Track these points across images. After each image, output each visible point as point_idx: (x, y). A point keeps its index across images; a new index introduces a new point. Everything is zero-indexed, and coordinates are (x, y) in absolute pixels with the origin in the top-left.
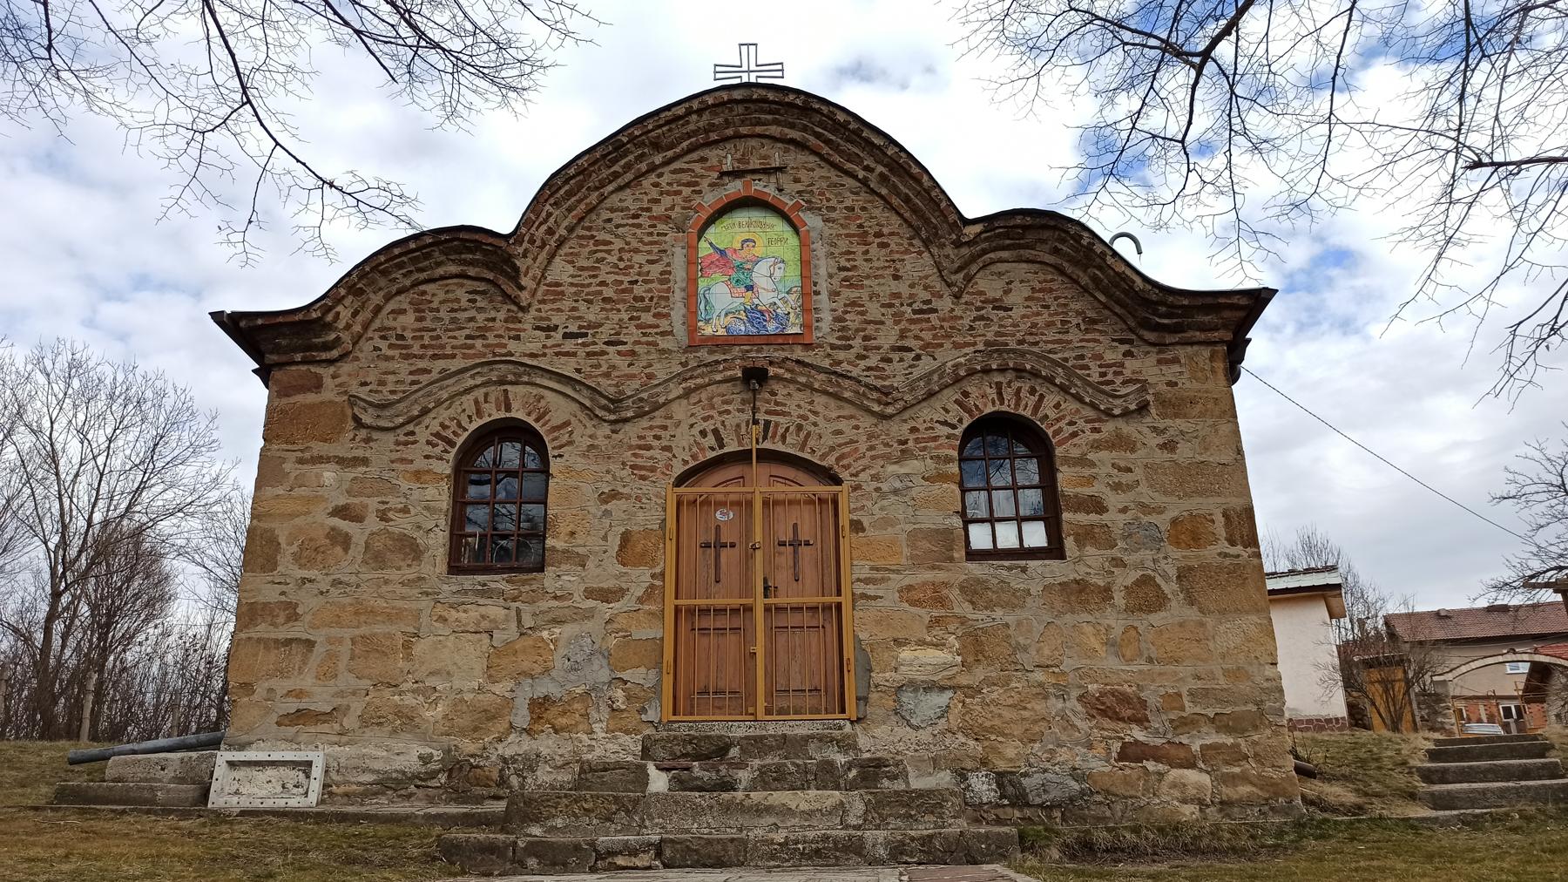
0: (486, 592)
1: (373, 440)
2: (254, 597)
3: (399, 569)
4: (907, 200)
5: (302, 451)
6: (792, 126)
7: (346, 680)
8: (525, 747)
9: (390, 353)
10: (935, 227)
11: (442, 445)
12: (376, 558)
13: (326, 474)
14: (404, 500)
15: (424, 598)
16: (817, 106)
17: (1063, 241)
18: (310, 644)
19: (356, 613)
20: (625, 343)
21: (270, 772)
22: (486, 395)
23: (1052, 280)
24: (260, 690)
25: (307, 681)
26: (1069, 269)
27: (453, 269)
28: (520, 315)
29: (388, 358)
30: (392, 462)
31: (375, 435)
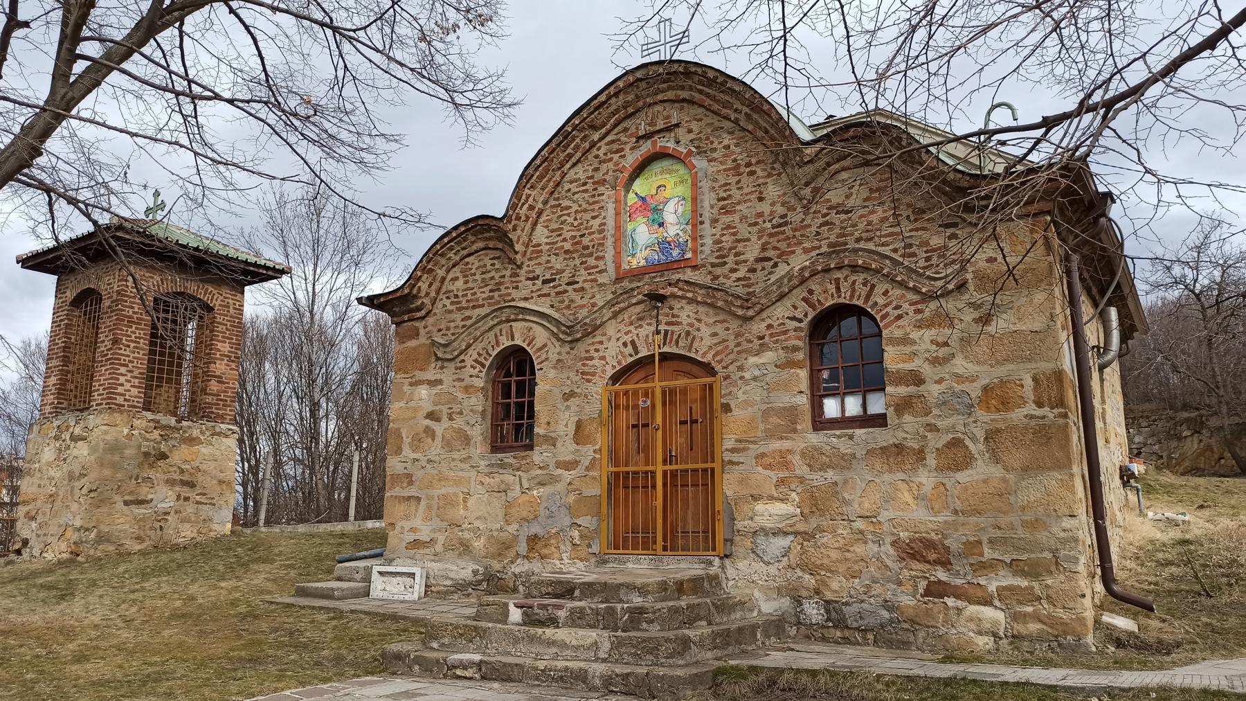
3: (459, 451)
13: (423, 392)
18: (418, 499)
22: (501, 330)
25: (417, 522)
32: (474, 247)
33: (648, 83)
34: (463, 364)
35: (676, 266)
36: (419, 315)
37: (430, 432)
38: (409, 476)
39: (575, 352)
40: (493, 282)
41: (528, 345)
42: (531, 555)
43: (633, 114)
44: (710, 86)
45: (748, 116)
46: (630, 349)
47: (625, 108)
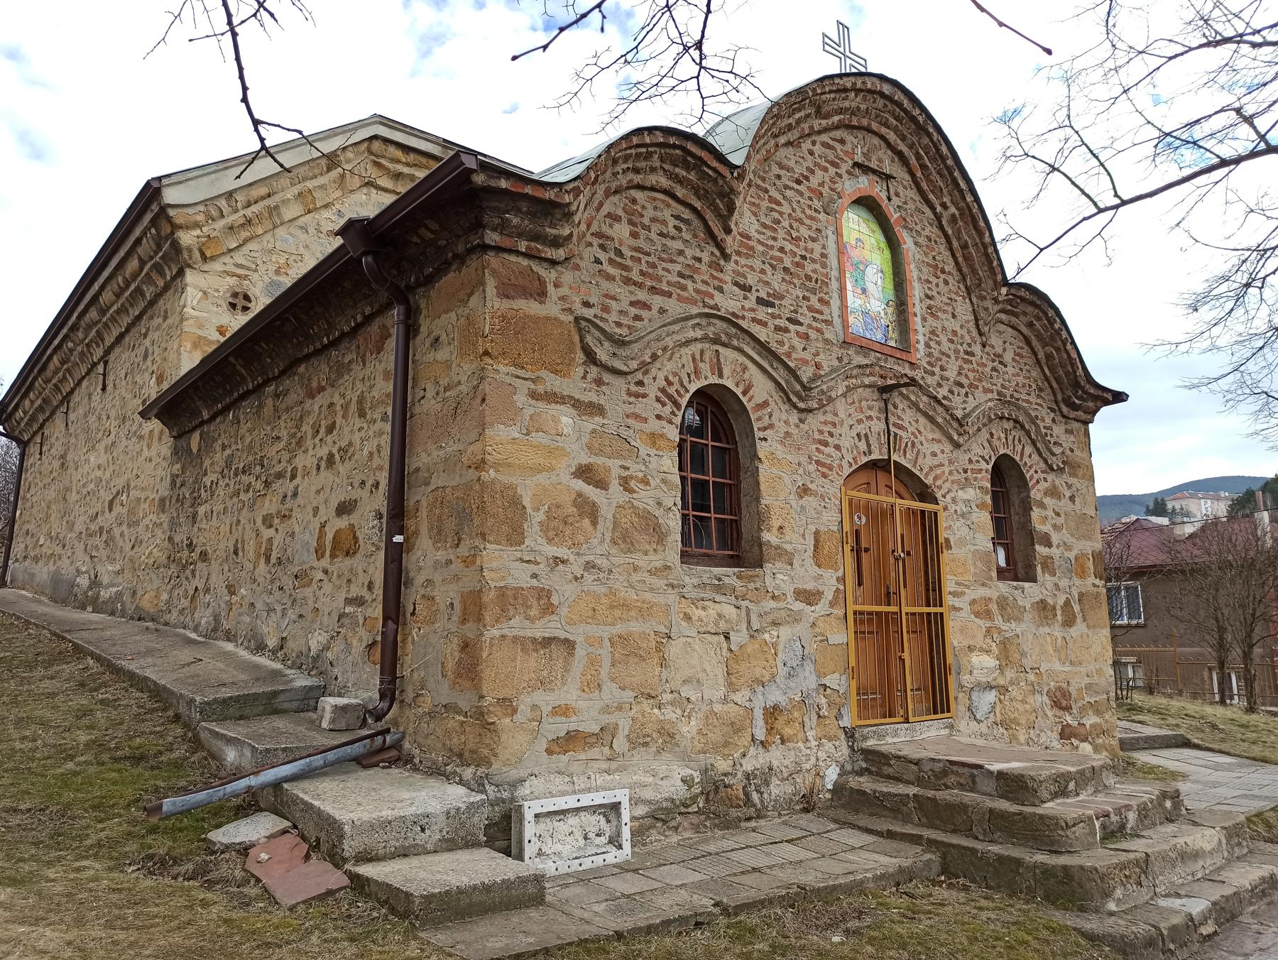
0: (720, 588)
1: (604, 384)
2: (503, 578)
3: (646, 553)
4: (964, 247)
5: (534, 381)
6: (903, 139)
7: (611, 692)
8: (761, 761)
9: (612, 271)
10: (980, 280)
11: (669, 408)
12: (624, 539)
13: (564, 419)
14: (643, 468)
15: (670, 590)
16: (931, 130)
17: (1039, 319)
18: (569, 645)
19: (612, 607)
20: (801, 324)
21: (572, 820)
22: (702, 352)
23: (1022, 348)
24: (524, 705)
25: (569, 694)
26: (1035, 342)
27: (664, 182)
28: (722, 262)
29: (610, 278)
30: (628, 416)
31: (607, 377)
32: (652, 179)
33: (885, 106)
34: (641, 390)
35: (898, 356)
36: (550, 253)
37: (590, 511)
38: (544, 594)
39: (805, 427)
40: (681, 259)
41: (744, 393)
42: (770, 739)
43: (854, 127)
44: (932, 160)
45: (953, 219)
46: (862, 446)
47: (853, 114)
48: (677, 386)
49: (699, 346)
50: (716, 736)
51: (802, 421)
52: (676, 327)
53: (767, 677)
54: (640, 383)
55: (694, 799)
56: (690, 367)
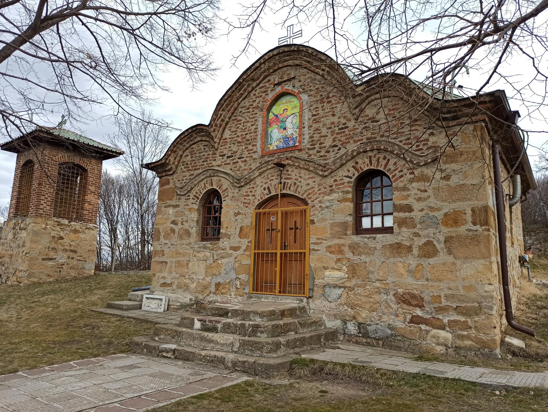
7: (174, 274)
12: (181, 237)
18: (166, 263)
25: (165, 274)
27: (199, 139)
33: (280, 57)
36: (170, 173)
46: (267, 191)
48: (199, 193)
49: (206, 179)
50: (199, 289)
51: (239, 191)
52: (197, 178)
53: (218, 273)
54: (189, 196)
55: (192, 305)
56: (203, 187)
